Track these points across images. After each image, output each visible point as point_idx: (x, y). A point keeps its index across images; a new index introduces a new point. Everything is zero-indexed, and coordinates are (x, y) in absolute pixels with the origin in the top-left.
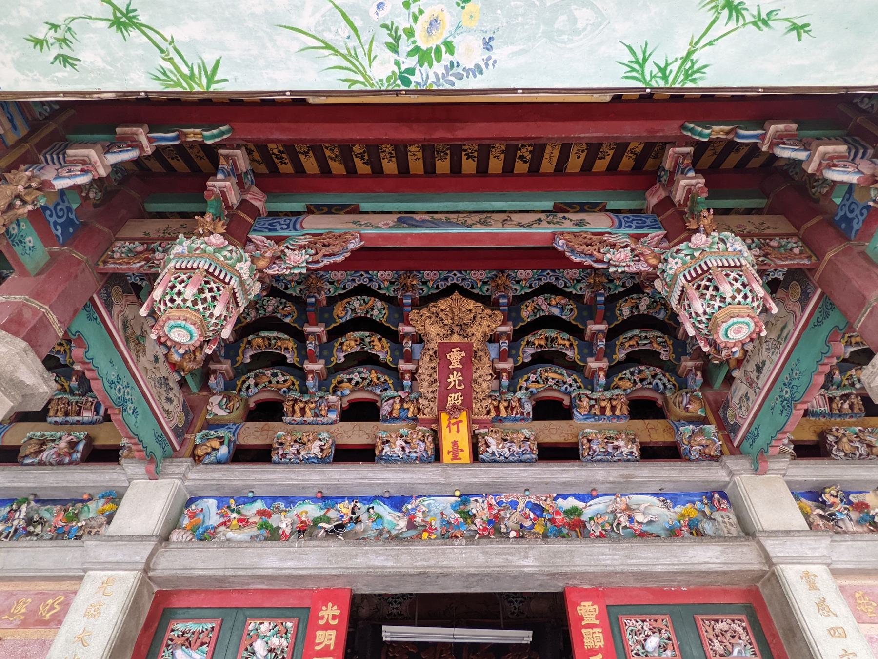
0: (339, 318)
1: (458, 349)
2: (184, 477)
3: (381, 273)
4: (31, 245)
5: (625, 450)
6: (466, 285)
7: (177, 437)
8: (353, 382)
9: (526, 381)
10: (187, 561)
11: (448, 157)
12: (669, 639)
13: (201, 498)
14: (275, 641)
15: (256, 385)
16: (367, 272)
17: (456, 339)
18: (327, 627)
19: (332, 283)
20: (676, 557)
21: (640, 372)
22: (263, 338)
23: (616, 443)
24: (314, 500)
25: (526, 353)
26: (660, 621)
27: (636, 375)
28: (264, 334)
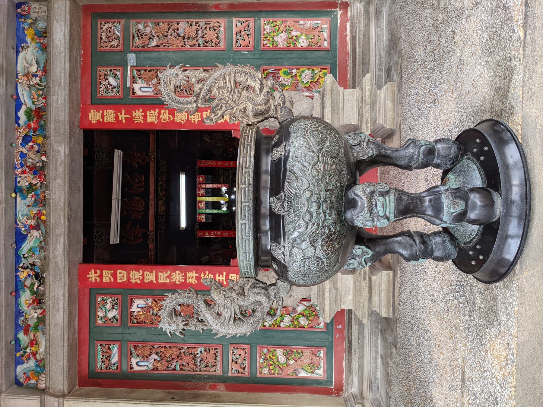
14: (108, 306)
18: (101, 276)
20: (60, 53)
26: (101, 74)
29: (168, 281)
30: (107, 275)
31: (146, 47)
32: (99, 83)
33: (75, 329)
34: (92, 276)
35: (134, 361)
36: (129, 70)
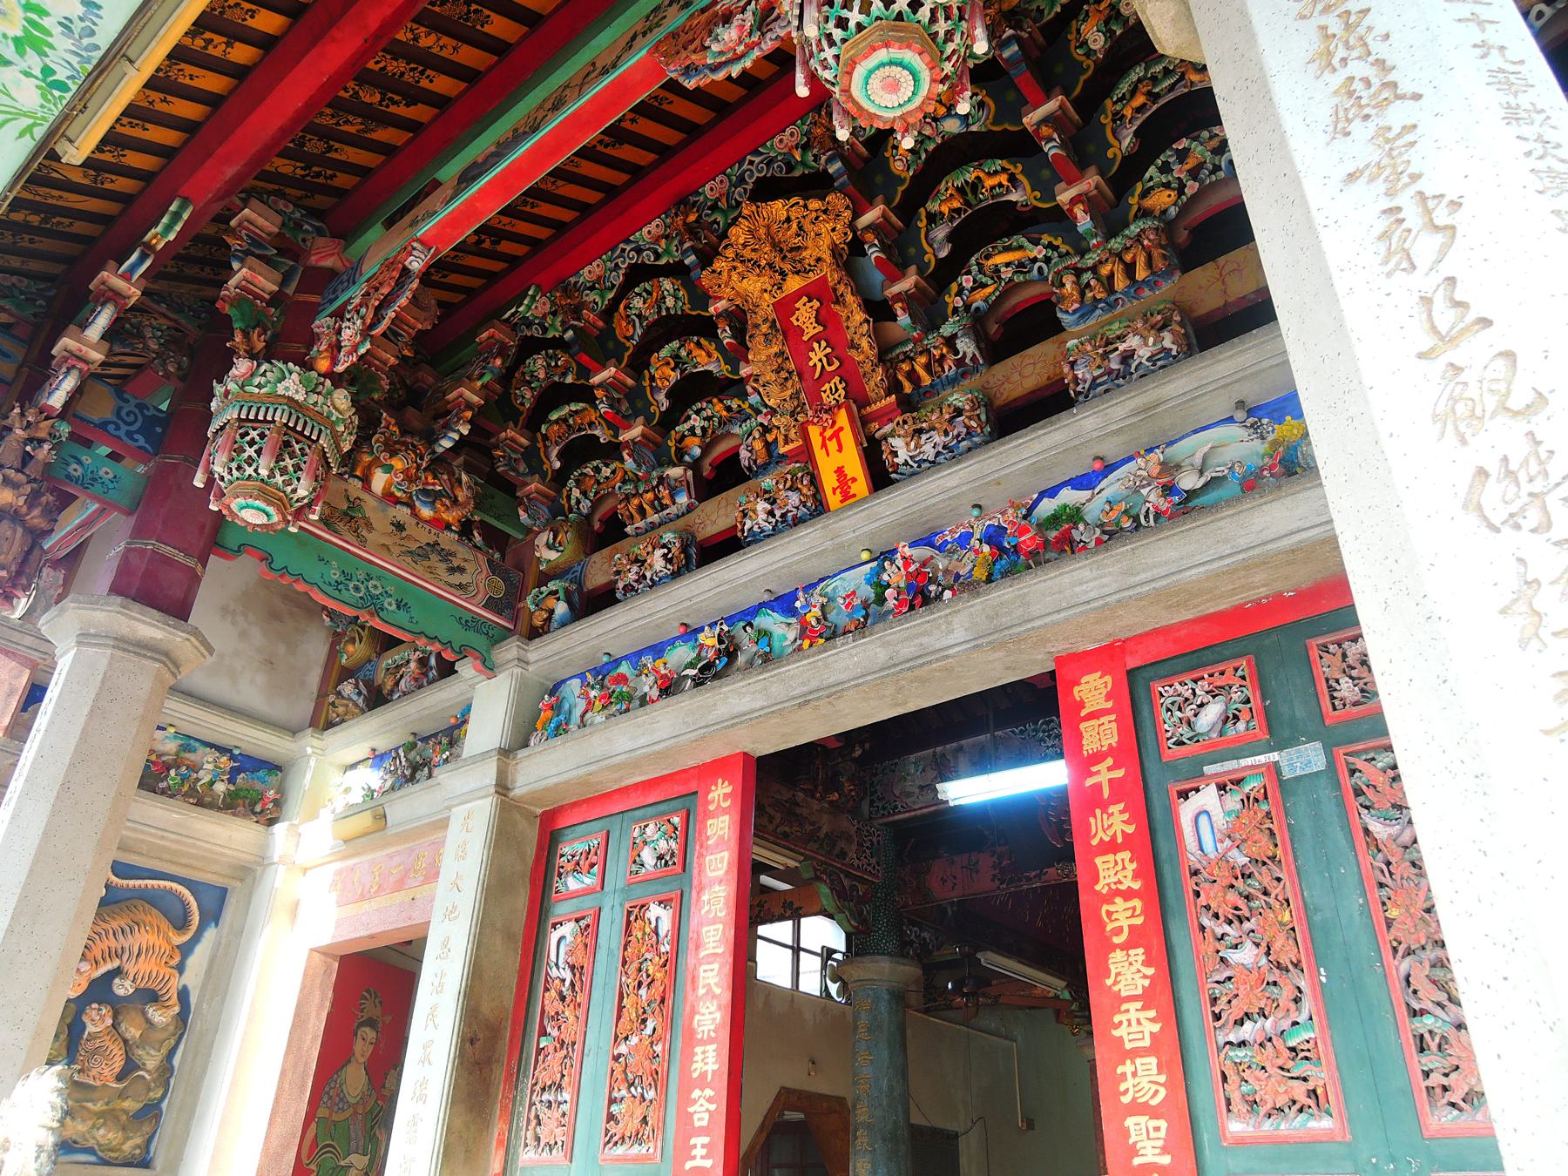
0: (628, 339)
1: (805, 299)
2: (523, 662)
3: (645, 230)
4: (111, 476)
5: (1144, 353)
6: (778, 170)
7: (499, 613)
8: (698, 431)
9: (960, 293)
10: (549, 769)
11: (486, 12)
13: (564, 681)
15: (584, 493)
16: (628, 241)
17: (794, 283)
19: (592, 288)
20: (1226, 541)
21: (1182, 155)
22: (556, 422)
23: (1122, 347)
25: (938, 242)
26: (1229, 672)
27: (1176, 167)
28: (554, 416)
29: (701, 992)
31: (1356, 803)
32: (1196, 675)
33: (621, 779)
36: (1262, 759)
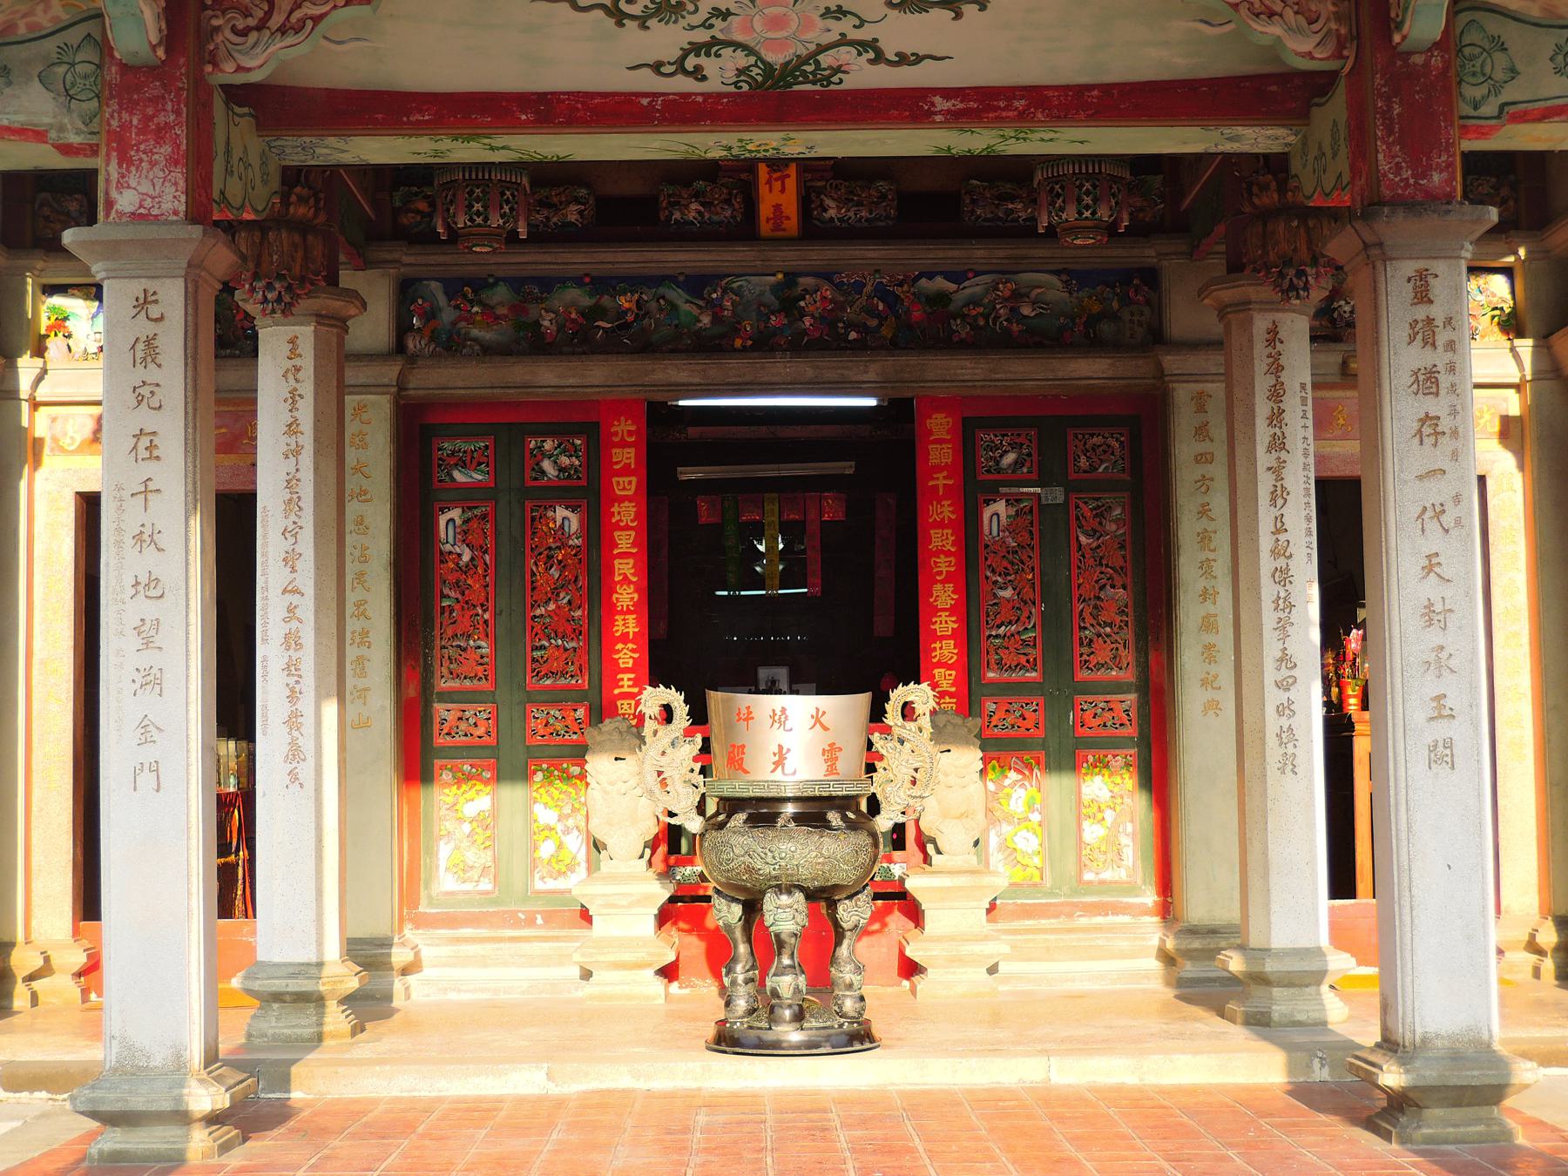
12: (1029, 455)
14: (565, 461)
18: (623, 444)
24: (578, 281)
30: (625, 456)
34: (623, 427)
35: (455, 514)
